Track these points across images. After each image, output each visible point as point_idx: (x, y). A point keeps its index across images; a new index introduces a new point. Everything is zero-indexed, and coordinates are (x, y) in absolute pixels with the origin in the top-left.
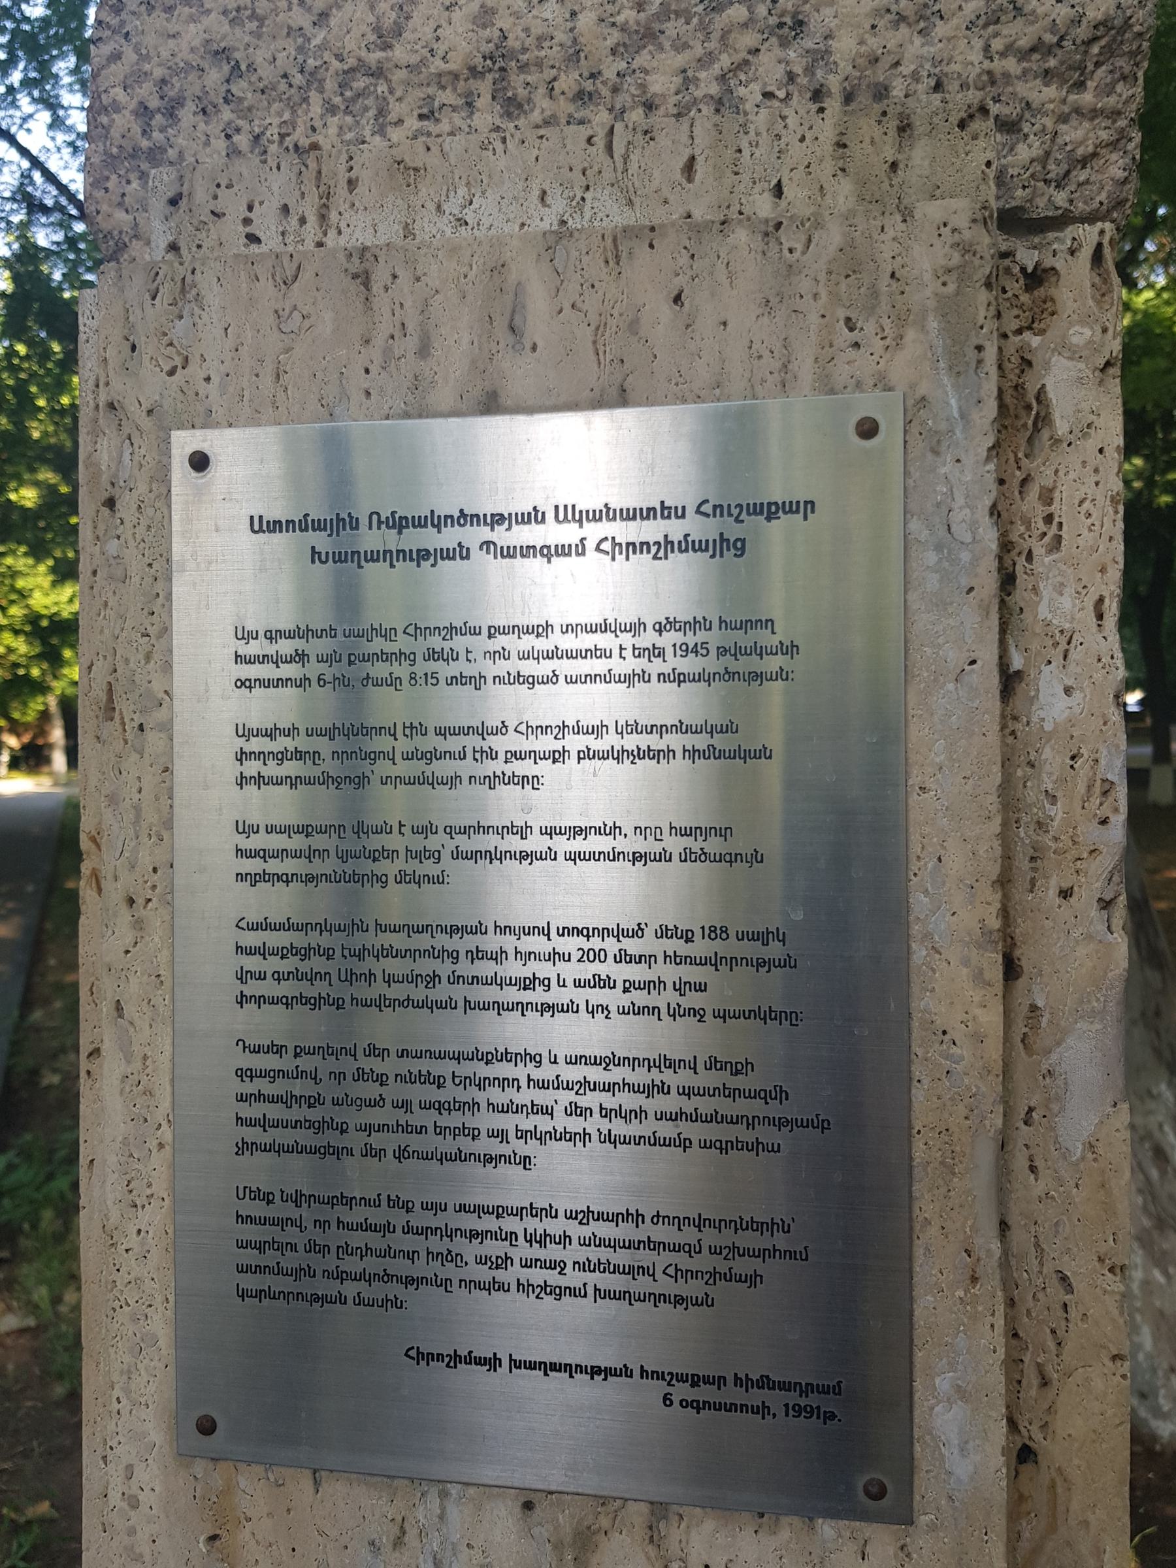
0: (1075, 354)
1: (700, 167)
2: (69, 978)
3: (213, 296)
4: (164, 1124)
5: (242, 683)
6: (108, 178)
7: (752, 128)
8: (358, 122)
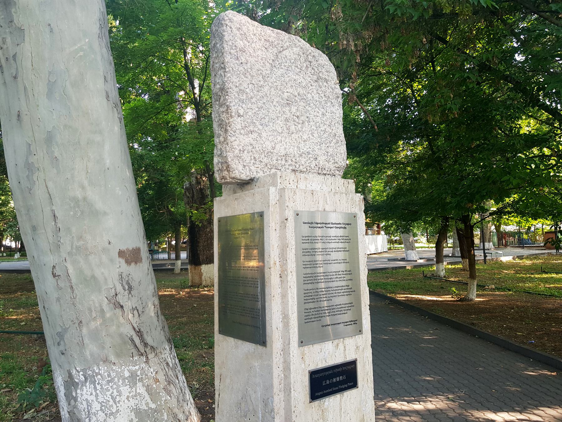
3: (298, 194)
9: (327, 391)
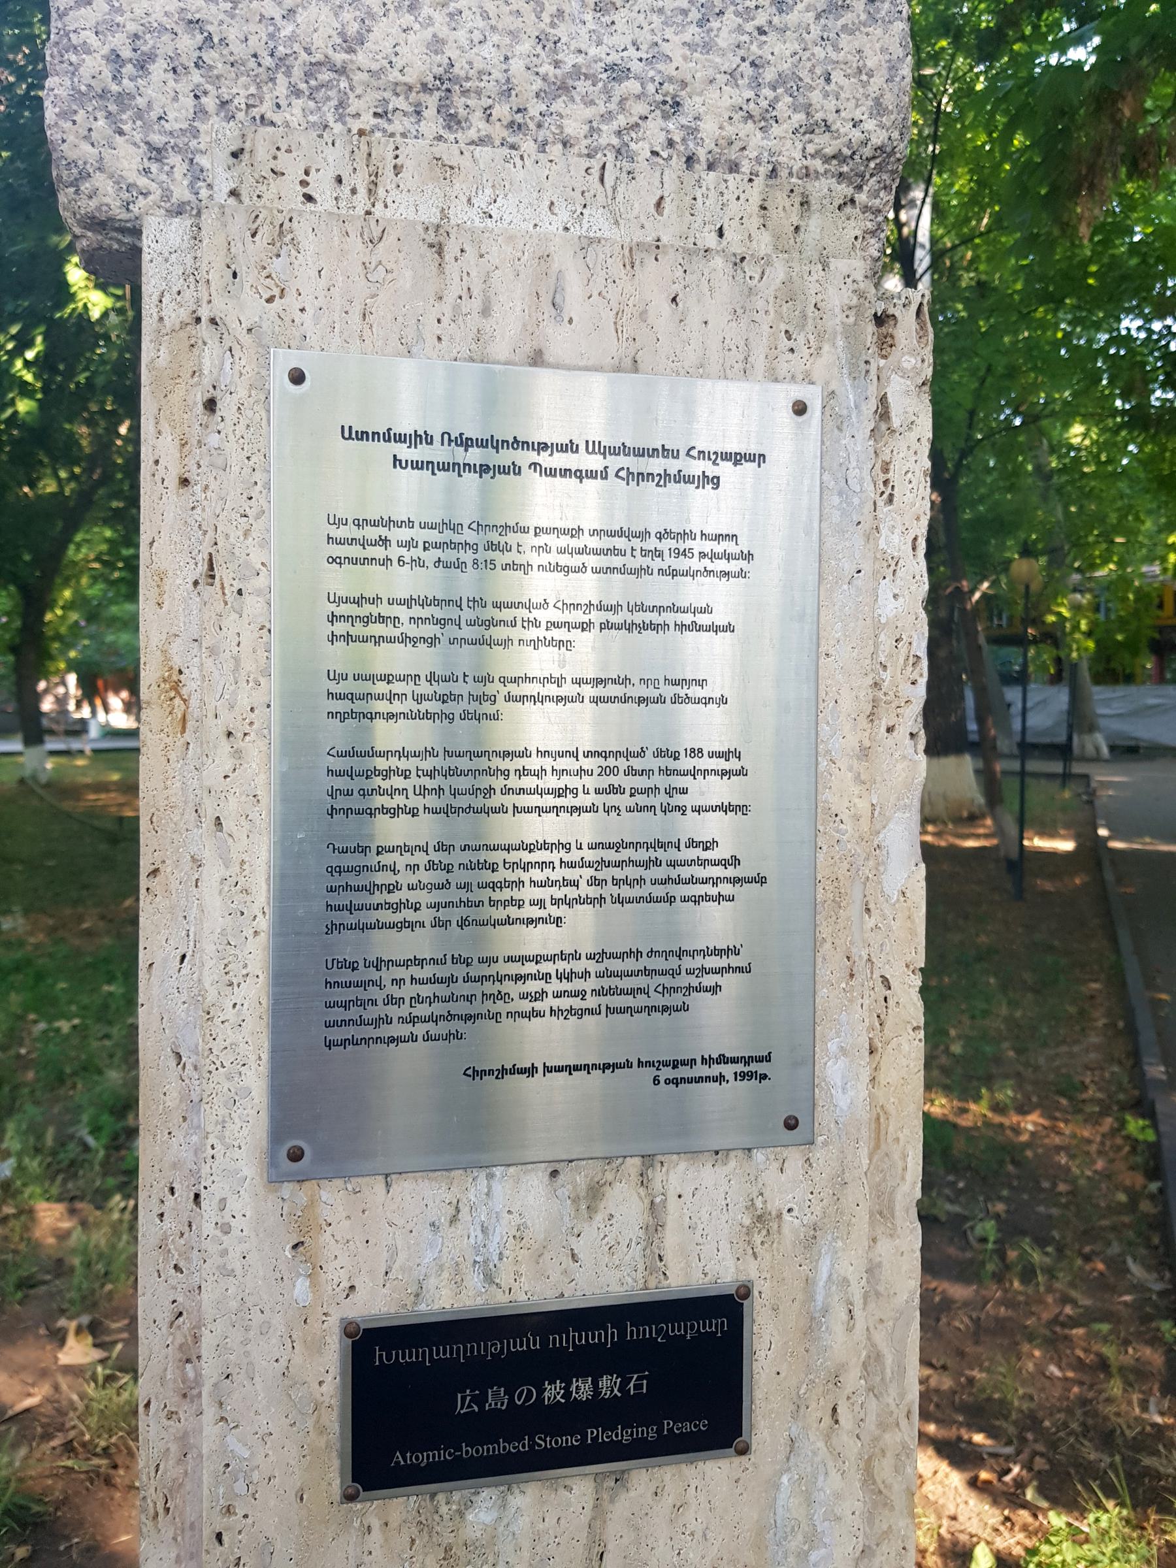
0: (905, 375)
1: (667, 204)
2: (129, 813)
3: (308, 243)
4: (260, 915)
5: (333, 560)
6: (75, 112)
7: (704, 184)
8: (319, 109)
9: (485, 1450)
